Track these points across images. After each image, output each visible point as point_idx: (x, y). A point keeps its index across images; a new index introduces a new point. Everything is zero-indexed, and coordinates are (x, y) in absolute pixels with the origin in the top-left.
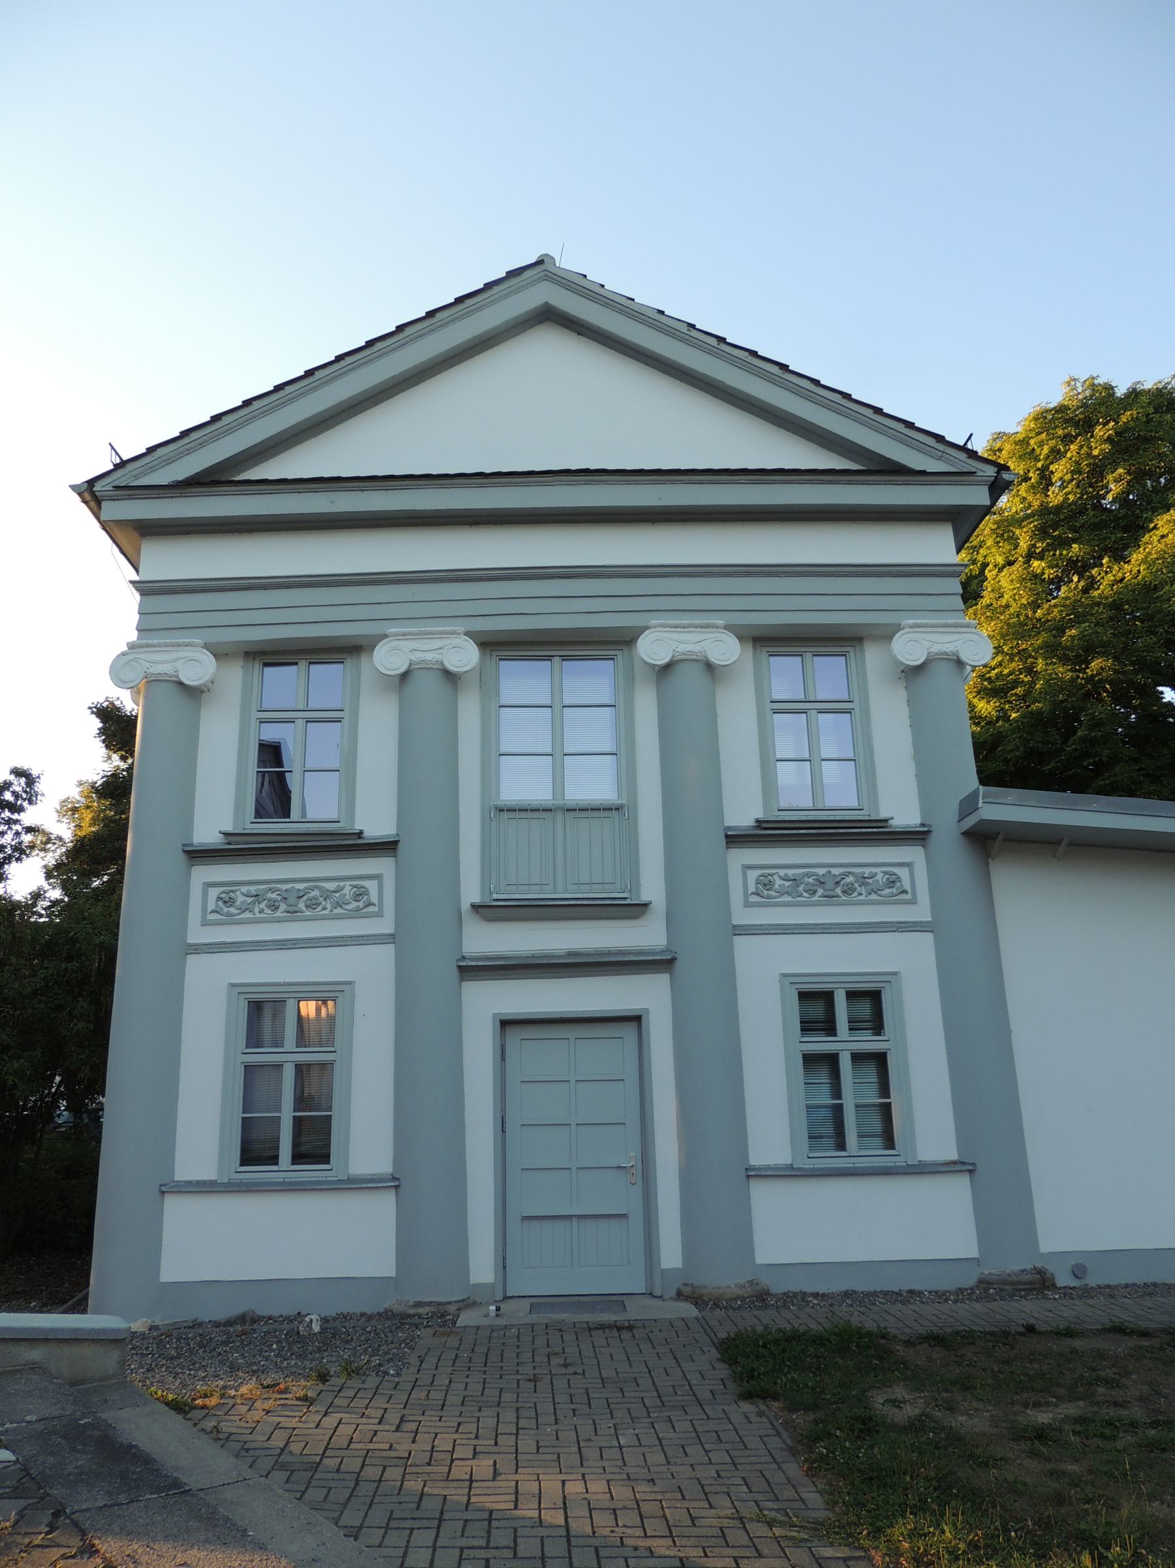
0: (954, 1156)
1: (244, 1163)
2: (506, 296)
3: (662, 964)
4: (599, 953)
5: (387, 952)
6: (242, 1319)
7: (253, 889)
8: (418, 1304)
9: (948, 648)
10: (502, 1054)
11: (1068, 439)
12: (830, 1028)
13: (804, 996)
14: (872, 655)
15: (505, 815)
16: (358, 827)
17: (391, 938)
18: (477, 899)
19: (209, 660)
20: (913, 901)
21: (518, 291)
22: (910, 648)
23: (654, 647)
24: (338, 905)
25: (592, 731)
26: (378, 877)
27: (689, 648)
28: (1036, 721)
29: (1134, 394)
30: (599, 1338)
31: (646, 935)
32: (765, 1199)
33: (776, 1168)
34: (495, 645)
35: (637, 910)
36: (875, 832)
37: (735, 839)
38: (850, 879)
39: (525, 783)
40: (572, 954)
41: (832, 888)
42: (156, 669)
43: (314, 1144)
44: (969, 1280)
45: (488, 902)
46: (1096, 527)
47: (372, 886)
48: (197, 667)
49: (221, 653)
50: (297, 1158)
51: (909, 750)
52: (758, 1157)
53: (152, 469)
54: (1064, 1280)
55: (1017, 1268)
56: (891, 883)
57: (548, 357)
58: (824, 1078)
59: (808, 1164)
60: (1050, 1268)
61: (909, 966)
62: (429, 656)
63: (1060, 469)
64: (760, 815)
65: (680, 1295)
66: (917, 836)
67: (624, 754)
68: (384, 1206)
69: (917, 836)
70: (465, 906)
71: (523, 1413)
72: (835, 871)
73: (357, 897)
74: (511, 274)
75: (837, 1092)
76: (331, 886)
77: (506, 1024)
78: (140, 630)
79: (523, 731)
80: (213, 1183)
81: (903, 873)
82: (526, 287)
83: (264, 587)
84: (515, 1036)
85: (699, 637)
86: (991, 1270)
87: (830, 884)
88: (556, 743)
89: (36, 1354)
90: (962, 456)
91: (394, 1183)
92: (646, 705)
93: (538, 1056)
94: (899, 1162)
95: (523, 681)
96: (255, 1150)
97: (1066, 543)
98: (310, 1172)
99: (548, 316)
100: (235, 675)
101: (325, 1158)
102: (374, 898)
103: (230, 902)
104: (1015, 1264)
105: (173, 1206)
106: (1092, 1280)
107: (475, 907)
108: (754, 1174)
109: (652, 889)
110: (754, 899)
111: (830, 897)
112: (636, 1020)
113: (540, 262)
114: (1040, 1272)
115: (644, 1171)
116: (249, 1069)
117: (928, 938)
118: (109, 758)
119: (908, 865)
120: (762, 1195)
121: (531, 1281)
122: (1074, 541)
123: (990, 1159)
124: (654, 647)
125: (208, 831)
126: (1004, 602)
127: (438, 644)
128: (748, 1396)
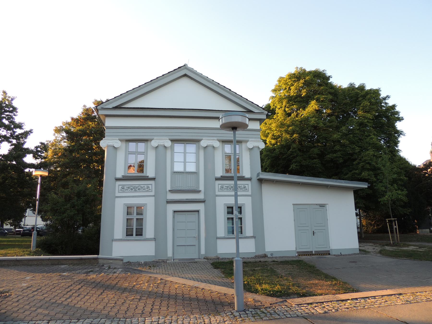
0: (252, 235)
1: (127, 236)
3: (203, 201)
4: (192, 199)
7: (128, 186)
9: (257, 145)
11: (294, 81)
12: (232, 213)
13: (228, 207)
14: (244, 145)
16: (244, 175)
17: (154, 196)
18: (170, 189)
19: (119, 142)
21: (180, 71)
22: (250, 145)
23: (204, 143)
24: (144, 189)
25: (191, 158)
26: (151, 184)
27: (210, 144)
28: (282, 147)
29: (310, 72)
30: (191, 263)
31: (200, 196)
34: (174, 141)
35: (199, 192)
37: (217, 179)
39: (178, 168)
40: (187, 199)
43: (140, 233)
44: (253, 256)
45: (171, 189)
46: (299, 102)
47: (150, 186)
49: (121, 140)
50: (136, 235)
51: (249, 163)
53: (108, 104)
54: (269, 256)
57: (185, 82)
58: (231, 221)
59: (227, 237)
60: (267, 254)
62: (162, 143)
63: (292, 88)
64: (222, 175)
65: (204, 258)
66: (249, 179)
67: (197, 162)
69: (249, 179)
70: (168, 190)
71: (155, 307)
73: (147, 188)
74: (179, 68)
75: (233, 225)
76: (143, 186)
77: (174, 212)
79: (178, 157)
80: (121, 239)
81: (247, 186)
83: (130, 128)
84: (176, 213)
85: (211, 141)
86: (257, 254)
88: (184, 160)
89: (111, 261)
90: (262, 109)
91: (155, 239)
92: (202, 153)
93: (181, 217)
94: (243, 236)
95: (179, 148)
96: (129, 233)
97: (293, 105)
99: (185, 75)
100: (124, 144)
101: (141, 235)
104: (261, 253)
105: (114, 243)
106: (274, 256)
107: (170, 191)
108: (218, 238)
109: (202, 188)
111: (135, 191)
112: (198, 211)
114: (265, 254)
116: (127, 219)
117: (250, 198)
118: (54, 135)
119: (248, 184)
120: (219, 241)
121: (179, 256)
122: (295, 105)
123: (258, 236)
124: (204, 143)
125: (119, 175)
126: (278, 118)
128: (215, 268)
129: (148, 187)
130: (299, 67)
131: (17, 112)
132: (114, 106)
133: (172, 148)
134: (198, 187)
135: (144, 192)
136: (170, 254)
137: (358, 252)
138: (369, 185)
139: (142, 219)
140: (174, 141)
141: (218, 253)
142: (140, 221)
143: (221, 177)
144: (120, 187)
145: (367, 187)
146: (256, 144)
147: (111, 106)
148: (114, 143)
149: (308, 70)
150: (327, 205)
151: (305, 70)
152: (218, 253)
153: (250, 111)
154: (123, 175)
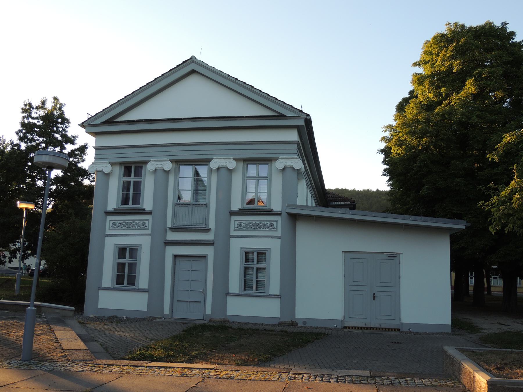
0: (278, 294)
1: (117, 284)
2: (182, 68)
3: (210, 244)
4: (198, 240)
5: (149, 238)
6: (113, 317)
7: (120, 222)
8: (150, 317)
9: (290, 164)
10: (174, 263)
15: (178, 206)
16: (272, 208)
18: (170, 226)
20: (276, 231)
24: (138, 226)
26: (148, 220)
29: (471, 29)
32: (230, 300)
33: (235, 293)
35: (208, 230)
36: (269, 213)
38: (261, 224)
41: (257, 227)
42: (99, 169)
43: (132, 281)
44: (277, 322)
47: (147, 222)
48: (107, 168)
50: (128, 284)
52: (231, 291)
54: (300, 324)
55: (286, 320)
56: (271, 226)
59: (243, 293)
61: (274, 247)
62: (160, 166)
66: (279, 214)
68: (277, 301)
69: (279, 214)
72: (257, 222)
73: (143, 225)
76: (137, 222)
77: (176, 257)
78: (95, 158)
81: (275, 223)
82: (188, 65)
84: (178, 260)
86: (281, 320)
87: (255, 226)
93: (182, 264)
96: (119, 280)
98: (131, 287)
101: (134, 284)
102: (147, 225)
103: (115, 225)
105: (101, 292)
106: (307, 325)
107: (170, 228)
109: (212, 225)
110: (236, 229)
111: (129, 228)
112: (205, 257)
113: (191, 58)
115: (204, 293)
125: (111, 207)
127: (163, 163)
129: (272, 225)
130: (452, 22)
131: (68, 122)
132: (103, 121)
133: (177, 172)
134: (207, 224)
135: (139, 229)
136: (167, 311)
137: (449, 330)
138: (469, 225)
139: (136, 264)
140: (178, 162)
141: (227, 314)
142: (133, 267)
143: (240, 210)
144: (112, 222)
145: (464, 227)
146: (289, 163)
147: (98, 122)
148: (103, 168)
149: (467, 25)
150: (401, 255)
151: (463, 26)
152: (227, 314)
153: (282, 116)
154: (115, 207)
